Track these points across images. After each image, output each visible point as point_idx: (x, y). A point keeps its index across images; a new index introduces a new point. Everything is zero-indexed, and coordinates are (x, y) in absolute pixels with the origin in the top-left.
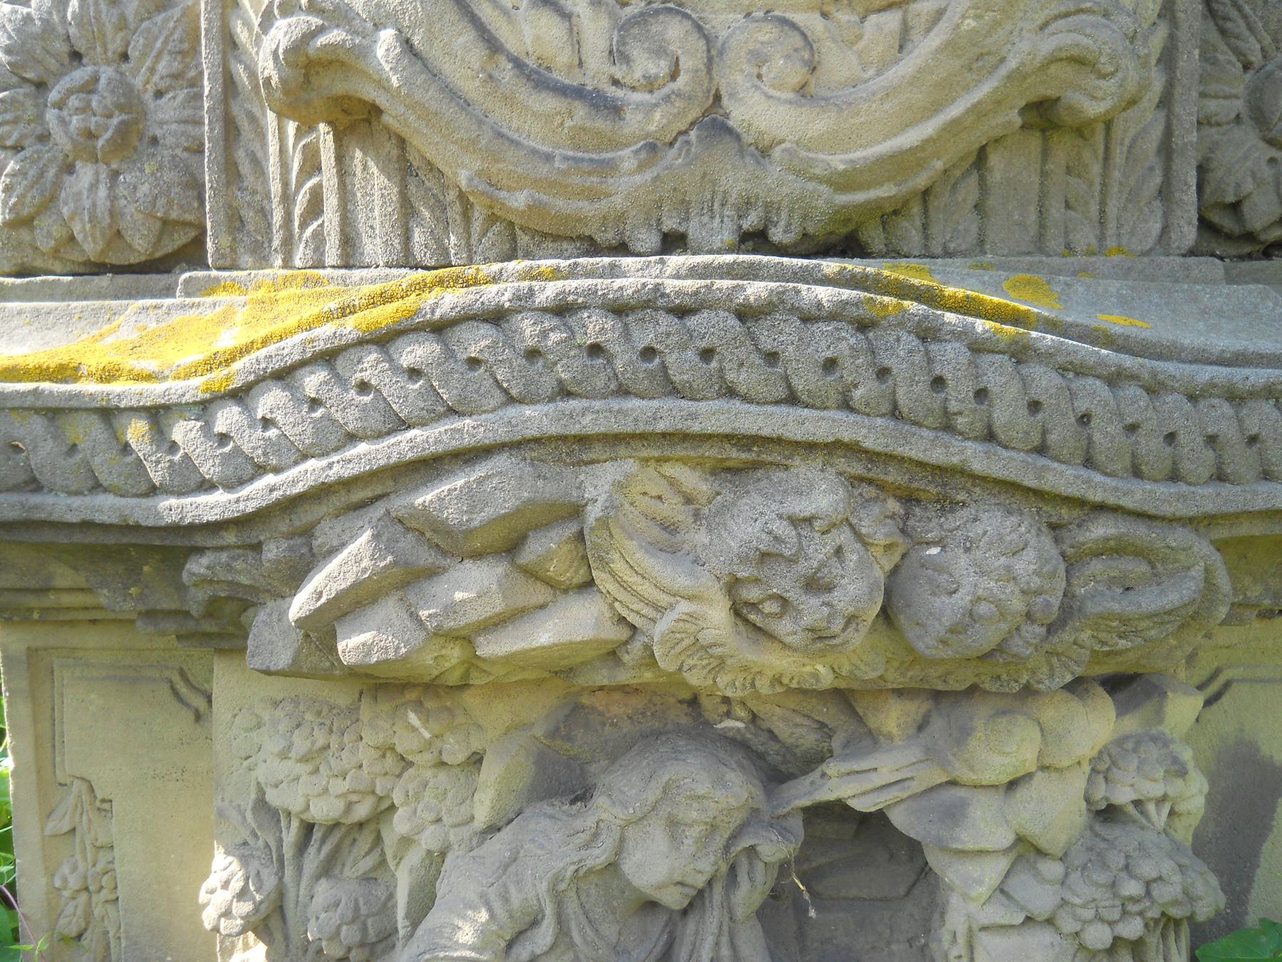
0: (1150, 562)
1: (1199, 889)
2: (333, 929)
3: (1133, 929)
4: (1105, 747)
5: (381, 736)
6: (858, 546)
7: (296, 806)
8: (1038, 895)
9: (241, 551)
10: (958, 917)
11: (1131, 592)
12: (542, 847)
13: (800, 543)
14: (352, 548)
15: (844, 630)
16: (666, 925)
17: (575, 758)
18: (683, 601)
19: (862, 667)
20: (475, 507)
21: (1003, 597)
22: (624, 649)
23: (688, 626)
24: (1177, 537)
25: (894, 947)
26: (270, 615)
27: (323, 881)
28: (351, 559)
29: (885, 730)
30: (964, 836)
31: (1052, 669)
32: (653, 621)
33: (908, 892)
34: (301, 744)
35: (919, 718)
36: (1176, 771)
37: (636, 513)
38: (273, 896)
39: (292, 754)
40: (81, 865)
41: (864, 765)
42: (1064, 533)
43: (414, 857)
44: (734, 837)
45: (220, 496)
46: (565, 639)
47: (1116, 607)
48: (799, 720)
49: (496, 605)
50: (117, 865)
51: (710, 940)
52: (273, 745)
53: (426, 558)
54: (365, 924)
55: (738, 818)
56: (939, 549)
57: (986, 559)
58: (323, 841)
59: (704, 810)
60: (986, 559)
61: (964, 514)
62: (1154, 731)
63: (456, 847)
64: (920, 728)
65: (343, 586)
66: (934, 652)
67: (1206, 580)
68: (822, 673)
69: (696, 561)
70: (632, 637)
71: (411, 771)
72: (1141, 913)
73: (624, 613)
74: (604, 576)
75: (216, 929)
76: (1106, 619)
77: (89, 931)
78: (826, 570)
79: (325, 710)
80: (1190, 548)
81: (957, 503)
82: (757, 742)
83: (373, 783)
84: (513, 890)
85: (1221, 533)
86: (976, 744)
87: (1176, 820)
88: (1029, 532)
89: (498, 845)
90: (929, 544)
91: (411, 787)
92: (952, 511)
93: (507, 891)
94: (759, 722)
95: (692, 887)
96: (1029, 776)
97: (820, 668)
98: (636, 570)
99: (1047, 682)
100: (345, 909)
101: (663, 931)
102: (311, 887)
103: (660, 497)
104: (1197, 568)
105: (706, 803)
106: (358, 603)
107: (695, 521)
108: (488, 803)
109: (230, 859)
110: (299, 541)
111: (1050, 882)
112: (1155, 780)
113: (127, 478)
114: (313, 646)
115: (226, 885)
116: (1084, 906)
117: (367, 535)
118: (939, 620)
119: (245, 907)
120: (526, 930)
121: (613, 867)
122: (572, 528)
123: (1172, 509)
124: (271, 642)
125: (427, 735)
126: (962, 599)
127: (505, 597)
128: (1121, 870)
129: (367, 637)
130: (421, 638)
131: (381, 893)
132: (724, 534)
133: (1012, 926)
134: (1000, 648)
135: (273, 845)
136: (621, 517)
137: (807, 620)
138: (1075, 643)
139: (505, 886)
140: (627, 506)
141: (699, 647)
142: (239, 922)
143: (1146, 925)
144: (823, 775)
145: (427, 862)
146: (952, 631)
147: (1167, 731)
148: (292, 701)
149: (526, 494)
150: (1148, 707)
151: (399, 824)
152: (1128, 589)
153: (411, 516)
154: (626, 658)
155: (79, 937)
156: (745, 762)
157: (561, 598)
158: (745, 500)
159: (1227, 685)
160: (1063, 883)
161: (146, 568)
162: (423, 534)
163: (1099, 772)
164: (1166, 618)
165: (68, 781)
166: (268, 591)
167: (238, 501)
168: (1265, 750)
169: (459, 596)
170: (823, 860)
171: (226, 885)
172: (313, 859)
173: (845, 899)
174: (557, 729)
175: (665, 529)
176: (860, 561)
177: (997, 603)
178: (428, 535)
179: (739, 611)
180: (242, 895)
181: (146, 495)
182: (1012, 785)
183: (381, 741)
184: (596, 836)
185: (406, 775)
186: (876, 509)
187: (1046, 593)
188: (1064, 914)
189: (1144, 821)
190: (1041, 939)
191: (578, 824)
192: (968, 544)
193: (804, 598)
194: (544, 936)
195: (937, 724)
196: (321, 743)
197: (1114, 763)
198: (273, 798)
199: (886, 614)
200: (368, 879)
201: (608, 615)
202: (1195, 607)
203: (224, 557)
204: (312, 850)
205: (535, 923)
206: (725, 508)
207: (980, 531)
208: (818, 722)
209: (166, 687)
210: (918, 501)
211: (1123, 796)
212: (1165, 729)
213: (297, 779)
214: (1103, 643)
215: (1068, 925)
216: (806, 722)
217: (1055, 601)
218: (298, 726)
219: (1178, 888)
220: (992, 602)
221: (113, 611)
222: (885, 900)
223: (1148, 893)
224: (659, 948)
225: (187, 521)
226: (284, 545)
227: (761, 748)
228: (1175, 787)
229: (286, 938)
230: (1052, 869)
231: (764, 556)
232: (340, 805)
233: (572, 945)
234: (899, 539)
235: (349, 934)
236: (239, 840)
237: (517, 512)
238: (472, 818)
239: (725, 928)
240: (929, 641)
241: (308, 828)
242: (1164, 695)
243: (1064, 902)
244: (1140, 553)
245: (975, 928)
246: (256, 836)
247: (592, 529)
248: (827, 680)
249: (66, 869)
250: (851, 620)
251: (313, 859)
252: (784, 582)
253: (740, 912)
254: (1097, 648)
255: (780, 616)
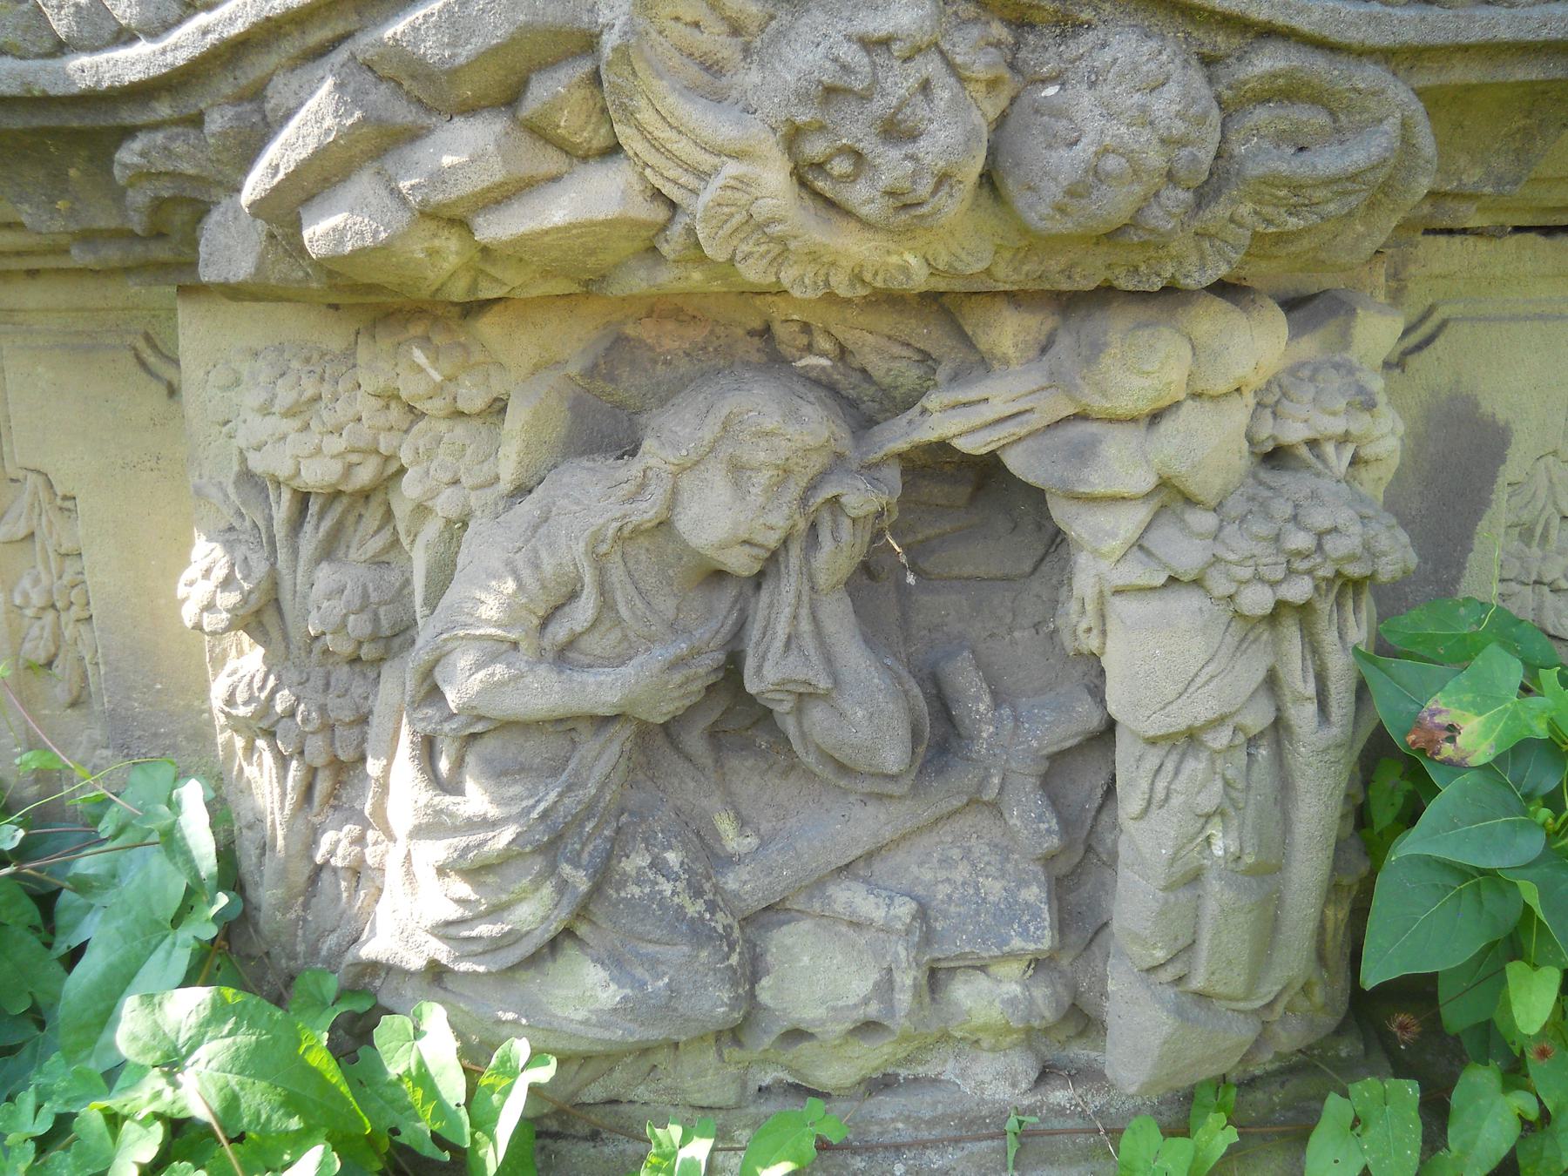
0: (1332, 113)
1: (1384, 542)
2: (338, 619)
3: (1298, 591)
4: (1275, 376)
5: (381, 379)
6: (952, 80)
7: (284, 470)
8: (1184, 550)
9: (180, 130)
10: (1088, 575)
11: (1305, 155)
12: (578, 502)
13: (875, 74)
14: (311, 104)
15: (934, 193)
16: (736, 602)
17: (620, 406)
18: (730, 162)
19: (963, 256)
20: (458, 37)
21: (1136, 147)
22: (662, 236)
23: (738, 195)
24: (1369, 75)
25: (1017, 634)
26: (225, 213)
27: (324, 565)
28: (313, 118)
29: (998, 352)
30: (1094, 478)
31: (1202, 258)
32: (694, 192)
33: (1035, 569)
34: (286, 396)
35: (1042, 338)
36: (1361, 403)
37: (666, 45)
38: (264, 585)
39: (276, 409)
40: (44, 577)
41: (973, 394)
42: (1220, 70)
43: (432, 529)
44: (813, 487)
45: (143, 48)
46: (584, 216)
47: (1283, 167)
48: (897, 350)
49: (494, 172)
50: (86, 577)
51: (787, 611)
52: (252, 398)
53: (404, 114)
54: (376, 614)
55: (817, 462)
56: (1057, 88)
57: (1116, 95)
58: (321, 515)
59: (774, 450)
60: (1116, 95)
61: (1089, 38)
62: (1337, 358)
63: (478, 513)
64: (1044, 350)
65: (304, 155)
66: (1048, 224)
67: (1405, 140)
68: (910, 266)
69: (745, 110)
70: (671, 220)
71: (422, 425)
72: (1310, 572)
73: (659, 183)
74: (629, 131)
75: (198, 627)
76: (1272, 185)
77: (61, 655)
78: (908, 111)
79: (315, 356)
80: (1383, 92)
81: (1081, 25)
82: (846, 383)
83: (376, 439)
84: (544, 554)
85: (1426, 79)
86: (1108, 361)
87: (1363, 470)
88: (1172, 61)
89: (528, 507)
90: (1045, 81)
91: (421, 443)
92: (1075, 35)
93: (537, 557)
94: (849, 359)
95: (761, 546)
96: (1177, 404)
97: (910, 259)
98: (673, 122)
99: (1196, 275)
100: (352, 594)
101: (732, 608)
102: (310, 573)
103: (697, 25)
104: (1391, 120)
105: (776, 440)
106: (326, 180)
107: (745, 58)
108: (514, 457)
109: (214, 545)
110: (248, 107)
111: (1200, 536)
112: (1334, 414)
113: (25, 32)
114: (280, 250)
115: (207, 573)
116: (1239, 564)
117: (329, 83)
118: (1055, 179)
119: (231, 598)
120: (563, 605)
121: (664, 525)
122: (584, 67)
123: (1360, 36)
124: (228, 247)
125: (438, 378)
126: (1085, 150)
127: (505, 162)
128: (1287, 521)
129: (338, 219)
130: (406, 220)
131: (394, 577)
132: (779, 66)
133: (1153, 589)
134: (1134, 223)
135: (261, 524)
136: (646, 48)
137: (885, 180)
138: (1232, 220)
139: (535, 551)
140: (654, 35)
141: (756, 226)
142: (225, 615)
143: (1317, 588)
144: (924, 411)
145: (446, 535)
146: (1071, 193)
147: (1355, 360)
148: (276, 349)
149: (522, 17)
150: (1331, 329)
151: (410, 488)
152: (1301, 149)
153: (382, 56)
154: (665, 249)
155: (49, 664)
156: (828, 401)
157: (580, 168)
158: (804, 20)
159: (1443, 325)
160: (1215, 538)
161: (73, 172)
162: (400, 85)
163: (1265, 406)
164: (1349, 186)
165: (20, 474)
166: (220, 183)
167: (164, 52)
168: (1486, 407)
169: (447, 160)
170: (931, 532)
171: (207, 573)
172: (310, 540)
173: (958, 578)
174: (596, 365)
175: (708, 69)
176: (953, 99)
177: (1129, 155)
178: (406, 84)
179: (804, 175)
180: (227, 583)
181: (51, 55)
182: (1155, 417)
183: (382, 385)
184: (643, 486)
185: (415, 429)
186: (975, 32)
187: (1193, 144)
188: (1215, 573)
189: (1320, 466)
190: (1187, 603)
191: (622, 474)
192: (1093, 78)
193: (881, 149)
194: (584, 611)
195: (1064, 342)
196: (310, 393)
197: (1284, 395)
198: (257, 463)
199: (989, 180)
200: (379, 562)
201: (638, 187)
202: (1386, 170)
203: (159, 137)
204: (308, 528)
205: (573, 596)
206: (781, 33)
207: (1109, 59)
208: (920, 351)
209: (129, 355)
210: (1032, 26)
211: (1294, 433)
212: (1352, 356)
213: (284, 438)
214: (1269, 222)
215: (1221, 587)
216: (906, 352)
217: (1206, 156)
218: (282, 375)
219: (1357, 541)
220: (1122, 155)
221: (40, 233)
222: (1006, 578)
223: (1320, 547)
224: (727, 627)
225: (106, 84)
226: (230, 112)
227: (853, 394)
228: (1359, 424)
229: (286, 637)
230: (1203, 520)
231: (830, 92)
232: (337, 467)
233: (619, 621)
234: (1007, 74)
235: (359, 626)
236: (223, 525)
237: (512, 42)
238: (497, 478)
239: (805, 599)
240: (1044, 209)
241: (303, 499)
242: (1352, 312)
243: (1216, 560)
244: (1318, 98)
245: (1107, 593)
246: (241, 515)
247: (609, 64)
248: (920, 280)
249: (26, 583)
250: (943, 179)
251: (310, 540)
252: (856, 129)
253: (822, 580)
254: (1260, 229)
255: (851, 178)
